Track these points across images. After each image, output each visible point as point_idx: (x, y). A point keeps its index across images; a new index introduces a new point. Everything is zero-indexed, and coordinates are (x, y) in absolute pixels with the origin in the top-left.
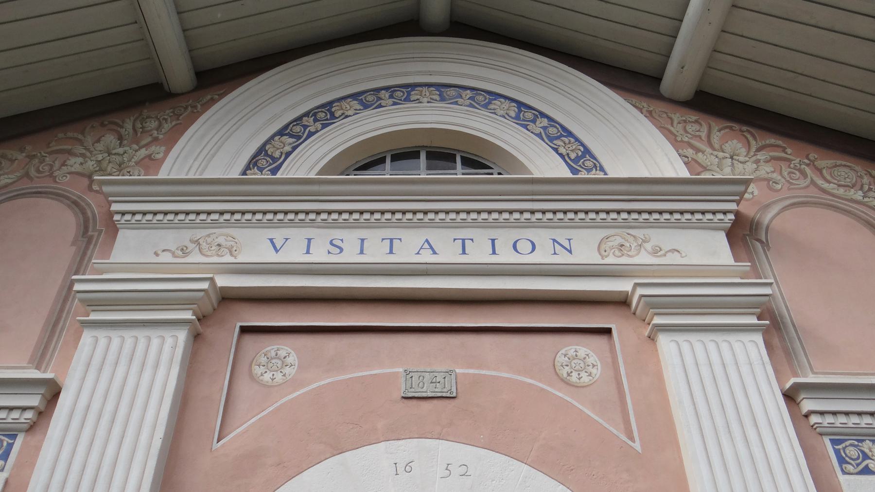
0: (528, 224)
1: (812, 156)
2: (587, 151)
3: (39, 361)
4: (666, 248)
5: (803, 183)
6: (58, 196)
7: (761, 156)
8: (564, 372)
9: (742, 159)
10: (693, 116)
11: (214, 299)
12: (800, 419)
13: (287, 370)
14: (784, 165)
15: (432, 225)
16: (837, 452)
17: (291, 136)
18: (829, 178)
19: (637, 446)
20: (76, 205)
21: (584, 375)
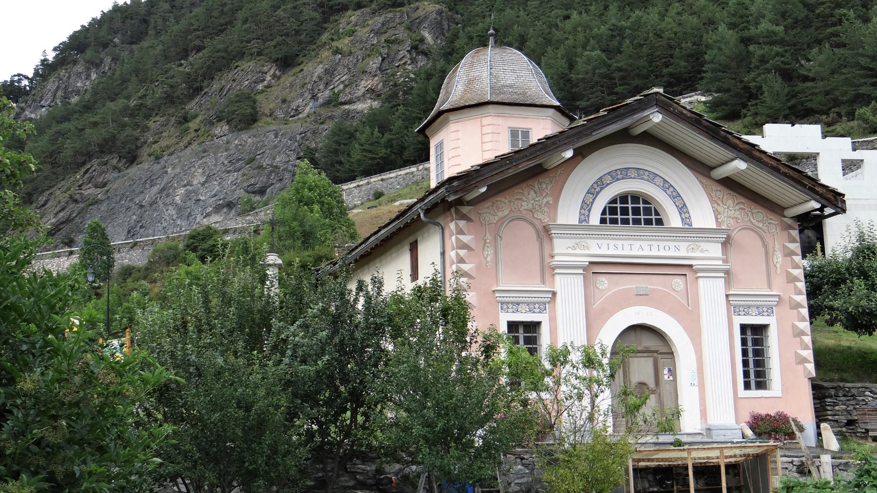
1: (752, 207)
2: (685, 204)
5: (747, 219)
10: (719, 187)
12: (728, 301)
14: (743, 211)
15: (642, 240)
20: (531, 224)
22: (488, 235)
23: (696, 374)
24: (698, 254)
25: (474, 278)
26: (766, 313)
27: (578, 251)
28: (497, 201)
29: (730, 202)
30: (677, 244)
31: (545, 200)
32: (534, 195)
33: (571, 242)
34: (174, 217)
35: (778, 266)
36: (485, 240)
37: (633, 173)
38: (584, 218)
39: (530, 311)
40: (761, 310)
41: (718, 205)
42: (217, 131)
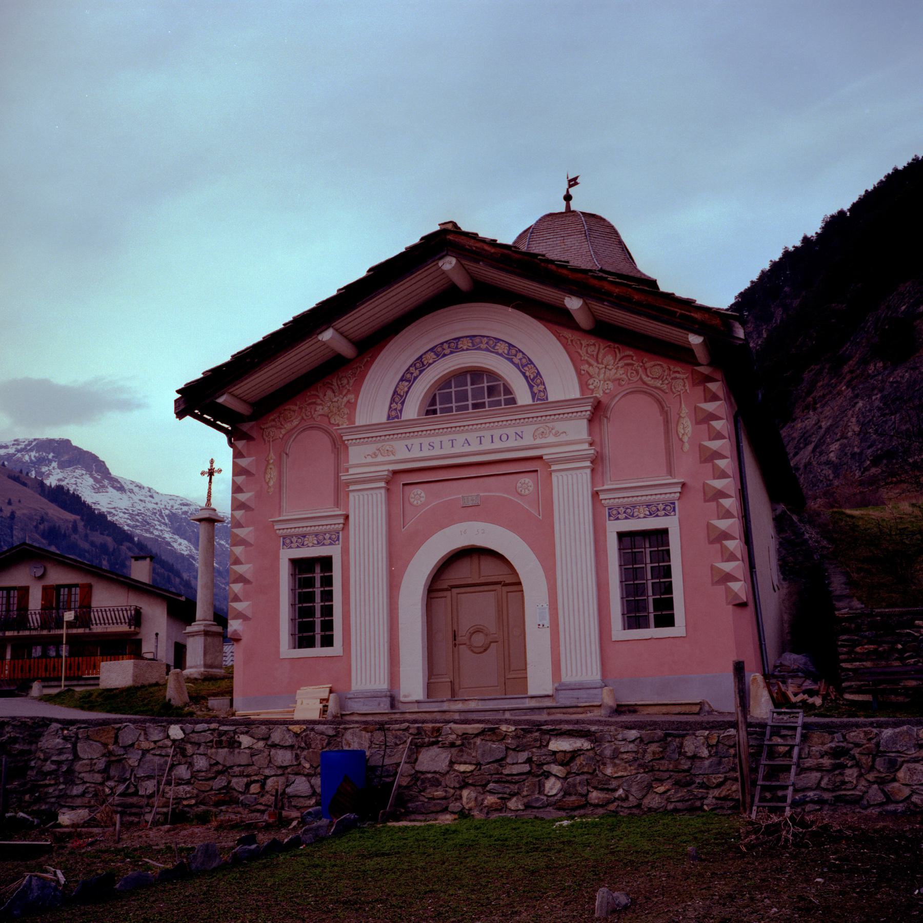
0: (505, 426)
2: (538, 373)
3: (337, 504)
4: (561, 431)
6: (319, 428)
7: (621, 364)
8: (519, 490)
9: (610, 367)
11: (391, 475)
13: (422, 499)
14: (629, 368)
16: (609, 513)
17: (407, 381)
18: (649, 374)
19: (540, 517)
20: (327, 432)
22: (272, 454)
23: (547, 610)
24: (551, 439)
25: (253, 510)
26: (663, 513)
27: (380, 459)
28: (285, 410)
29: (609, 359)
30: (519, 430)
31: (345, 399)
32: (332, 395)
33: (370, 448)
34: (831, 478)
35: (686, 439)
36: (268, 461)
37: (466, 344)
38: (394, 414)
39: (318, 543)
40: (654, 509)
41: (590, 365)
42: (871, 369)
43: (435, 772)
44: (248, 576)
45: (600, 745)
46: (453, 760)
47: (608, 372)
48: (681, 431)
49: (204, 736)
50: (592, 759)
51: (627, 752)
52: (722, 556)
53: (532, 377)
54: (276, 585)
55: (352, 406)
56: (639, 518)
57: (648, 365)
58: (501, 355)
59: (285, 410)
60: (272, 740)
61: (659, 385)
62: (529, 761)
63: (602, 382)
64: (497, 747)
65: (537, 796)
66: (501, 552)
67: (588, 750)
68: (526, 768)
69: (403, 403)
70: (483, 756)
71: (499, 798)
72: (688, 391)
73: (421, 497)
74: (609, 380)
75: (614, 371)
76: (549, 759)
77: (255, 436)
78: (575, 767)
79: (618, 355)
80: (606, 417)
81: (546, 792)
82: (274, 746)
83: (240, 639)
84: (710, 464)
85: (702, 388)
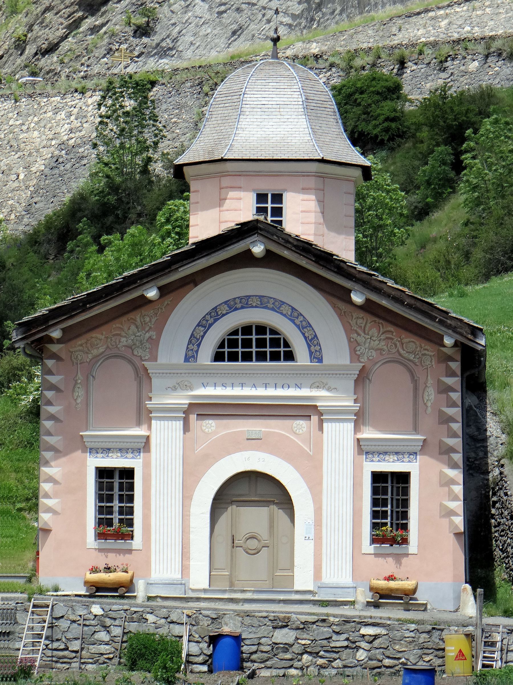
2: (316, 336)
4: (332, 388)
5: (394, 351)
9: (374, 339)
13: (212, 428)
14: (390, 341)
18: (405, 348)
20: (130, 362)
21: (300, 430)
28: (92, 337)
29: (374, 331)
31: (147, 335)
35: (429, 404)
36: (76, 381)
41: (359, 335)
43: (286, 644)
44: (57, 477)
45: (393, 632)
46: (298, 637)
47: (372, 342)
48: (426, 397)
49: (119, 614)
50: (386, 640)
51: (409, 637)
52: (449, 496)
53: (310, 338)
54: (83, 487)
55: (155, 342)
56: (389, 462)
57: (405, 340)
58: (285, 315)
59: (92, 337)
60: (171, 618)
61: (412, 358)
62: (347, 639)
63: (367, 350)
64: (326, 631)
65: (351, 660)
66: (277, 478)
67: (384, 635)
68: (345, 643)
69: (199, 345)
70: (317, 635)
71: (327, 661)
72: (434, 366)
73: (211, 426)
74: (373, 349)
75: (377, 342)
76: (360, 639)
77: (64, 358)
78: (376, 643)
79: (381, 329)
80: (369, 379)
81: (357, 658)
82: (172, 622)
83: (50, 531)
84: (446, 426)
85: (445, 365)
